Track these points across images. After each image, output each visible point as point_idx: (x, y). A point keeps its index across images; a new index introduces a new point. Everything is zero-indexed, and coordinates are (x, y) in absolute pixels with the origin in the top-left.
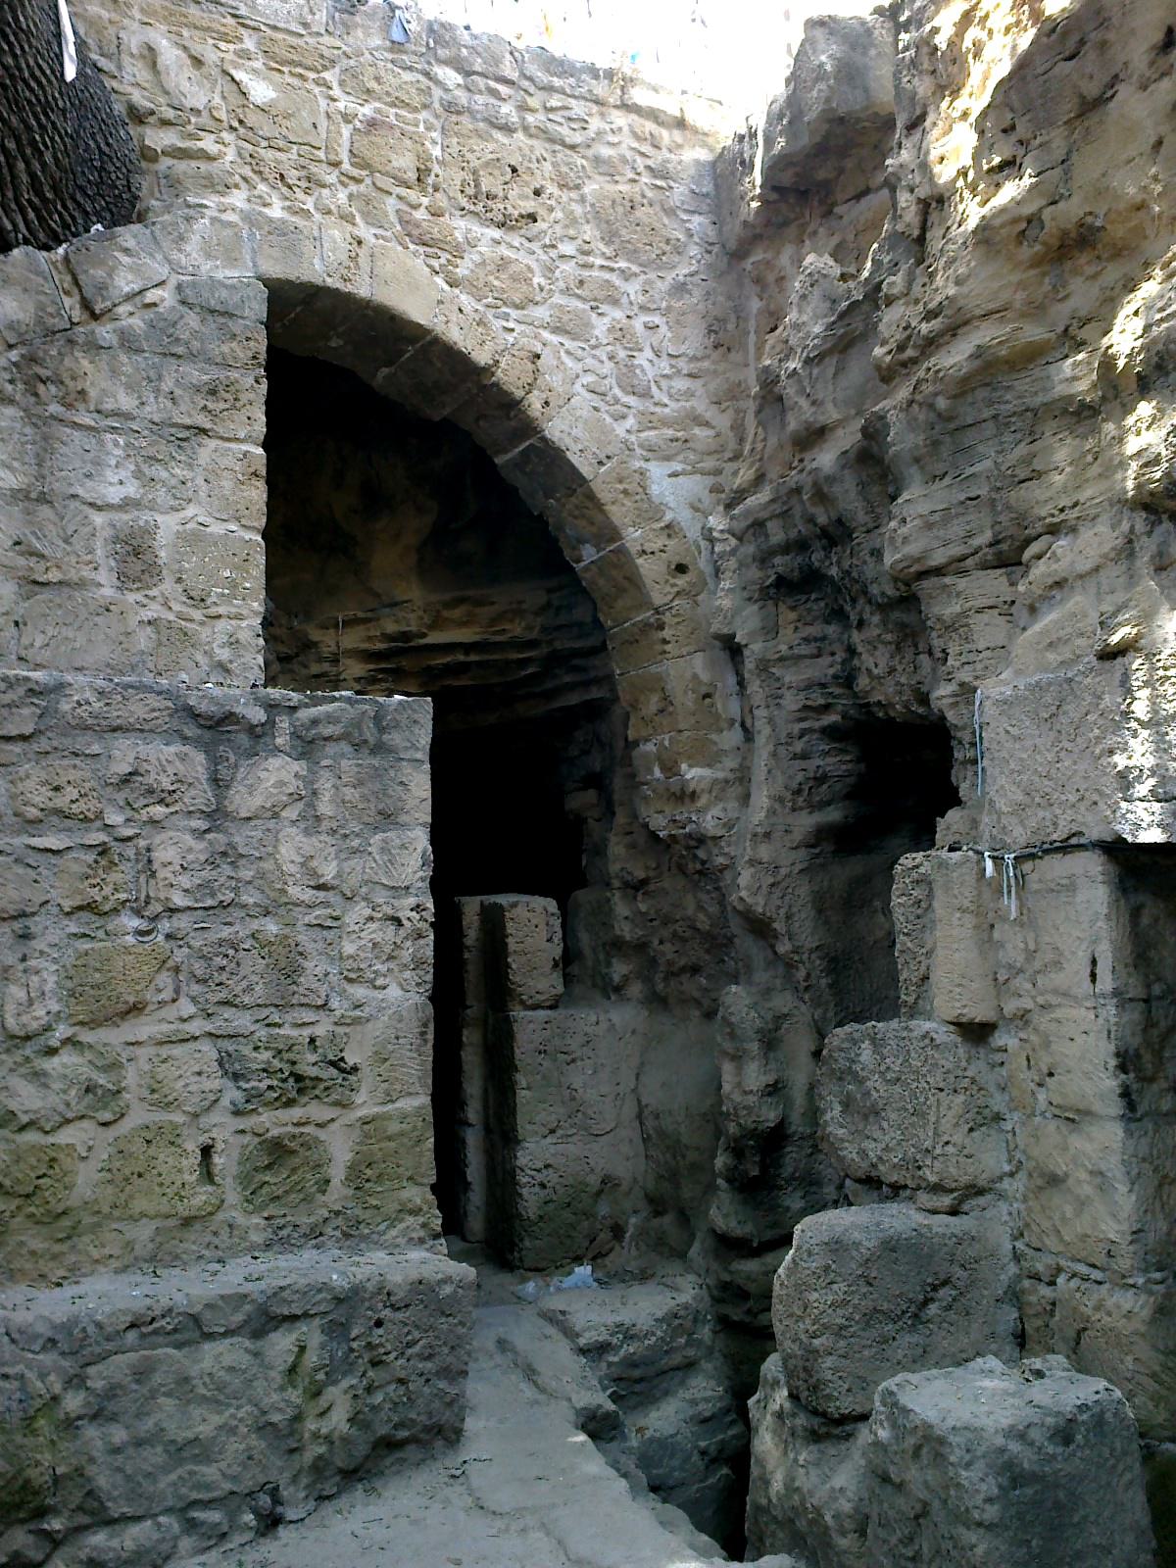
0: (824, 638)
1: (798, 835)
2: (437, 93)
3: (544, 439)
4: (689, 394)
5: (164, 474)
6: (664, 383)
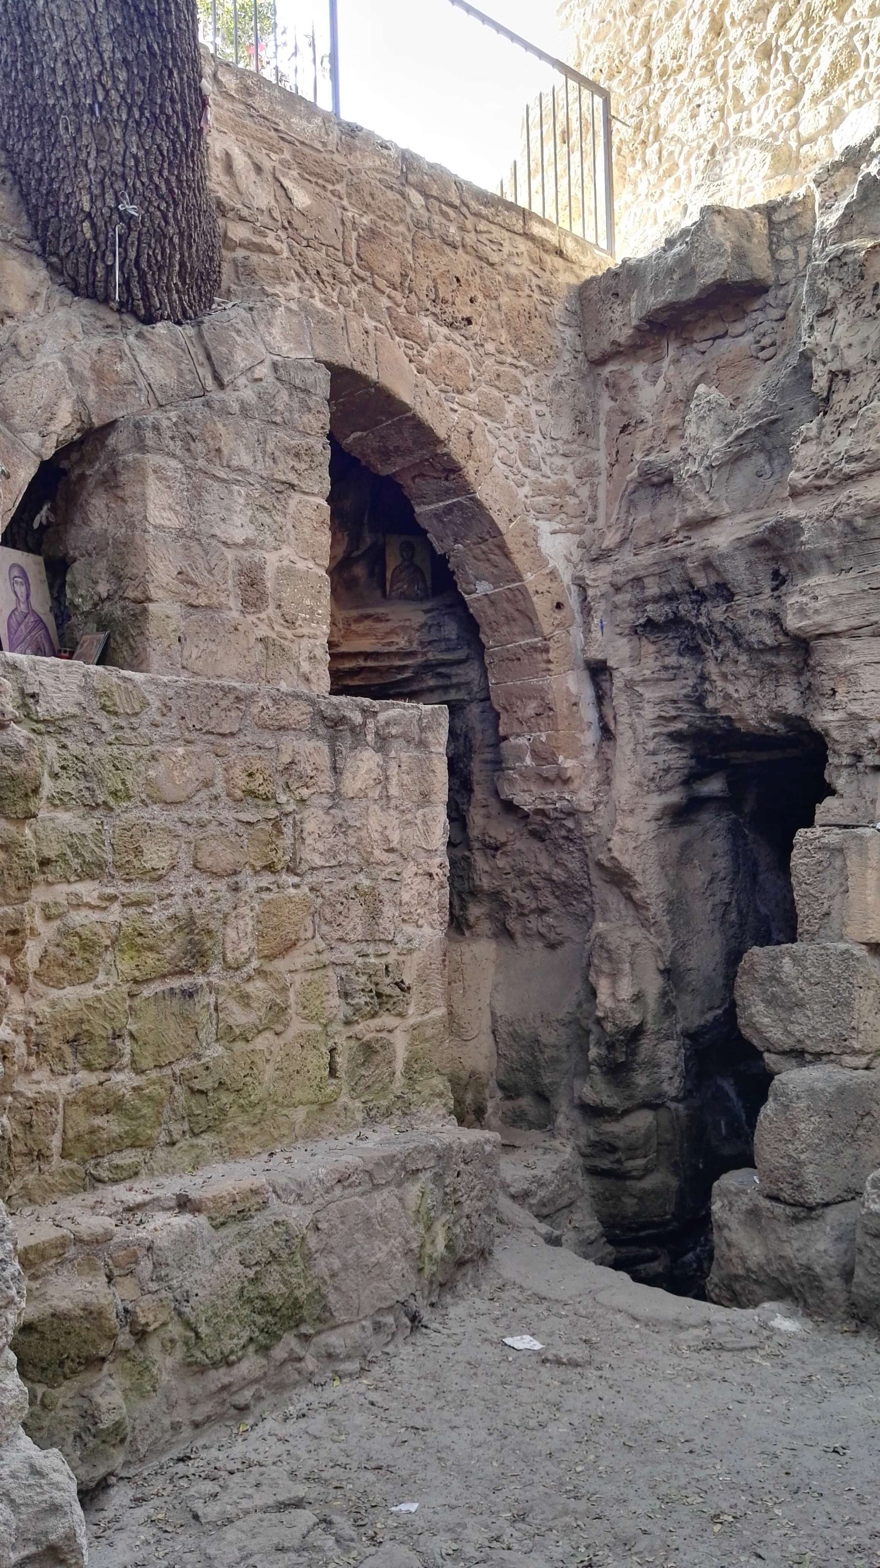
0: (680, 667)
1: (652, 812)
2: (409, 210)
3: (474, 500)
4: (564, 469)
5: (269, 521)
6: (548, 459)
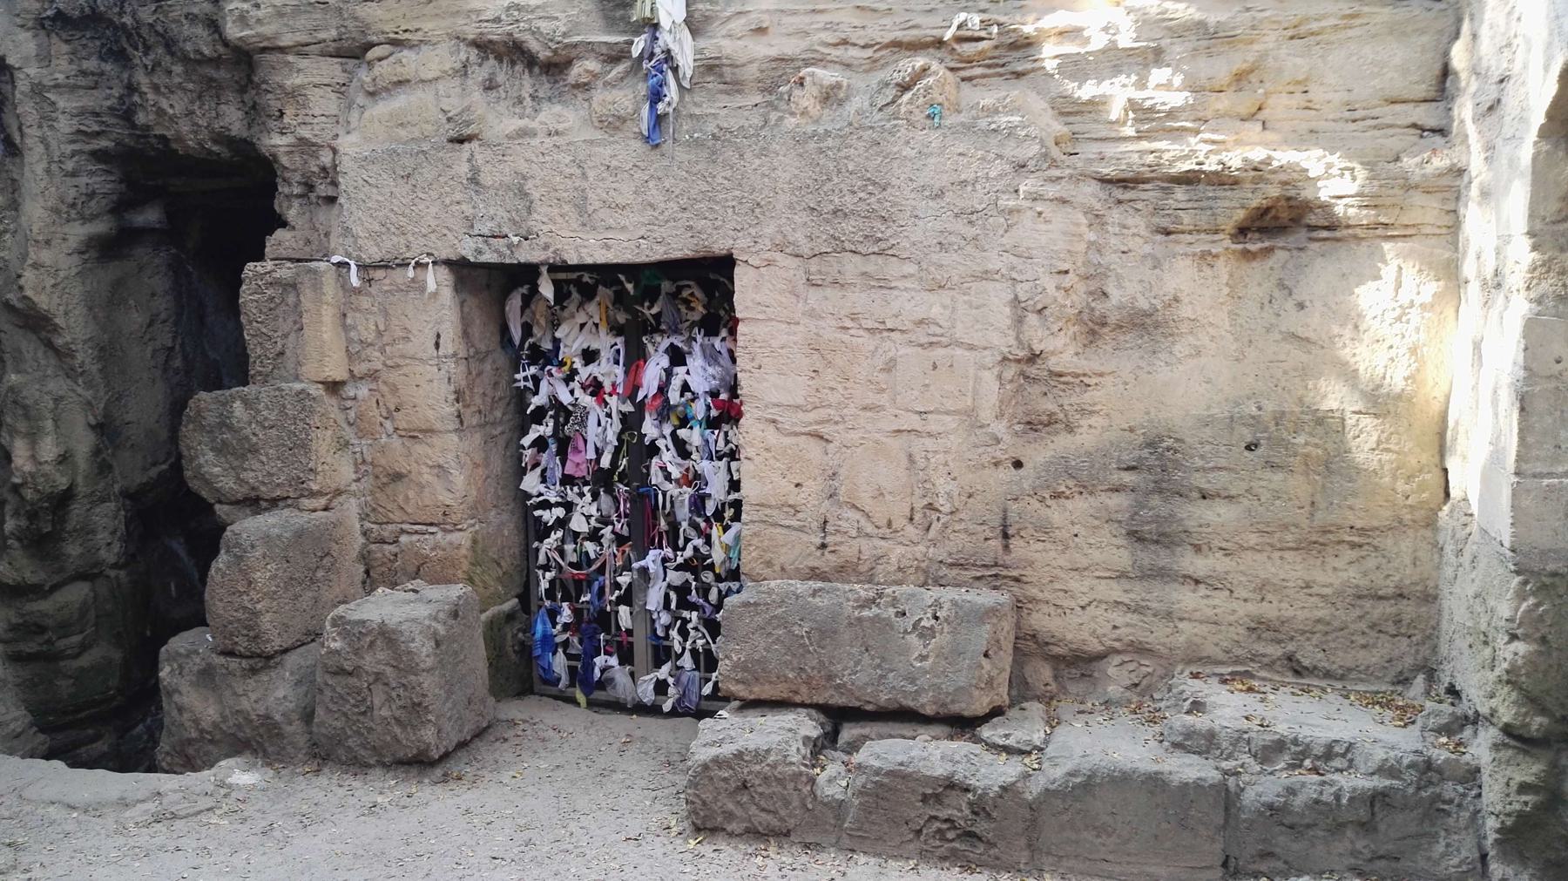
1: (73, 242)
